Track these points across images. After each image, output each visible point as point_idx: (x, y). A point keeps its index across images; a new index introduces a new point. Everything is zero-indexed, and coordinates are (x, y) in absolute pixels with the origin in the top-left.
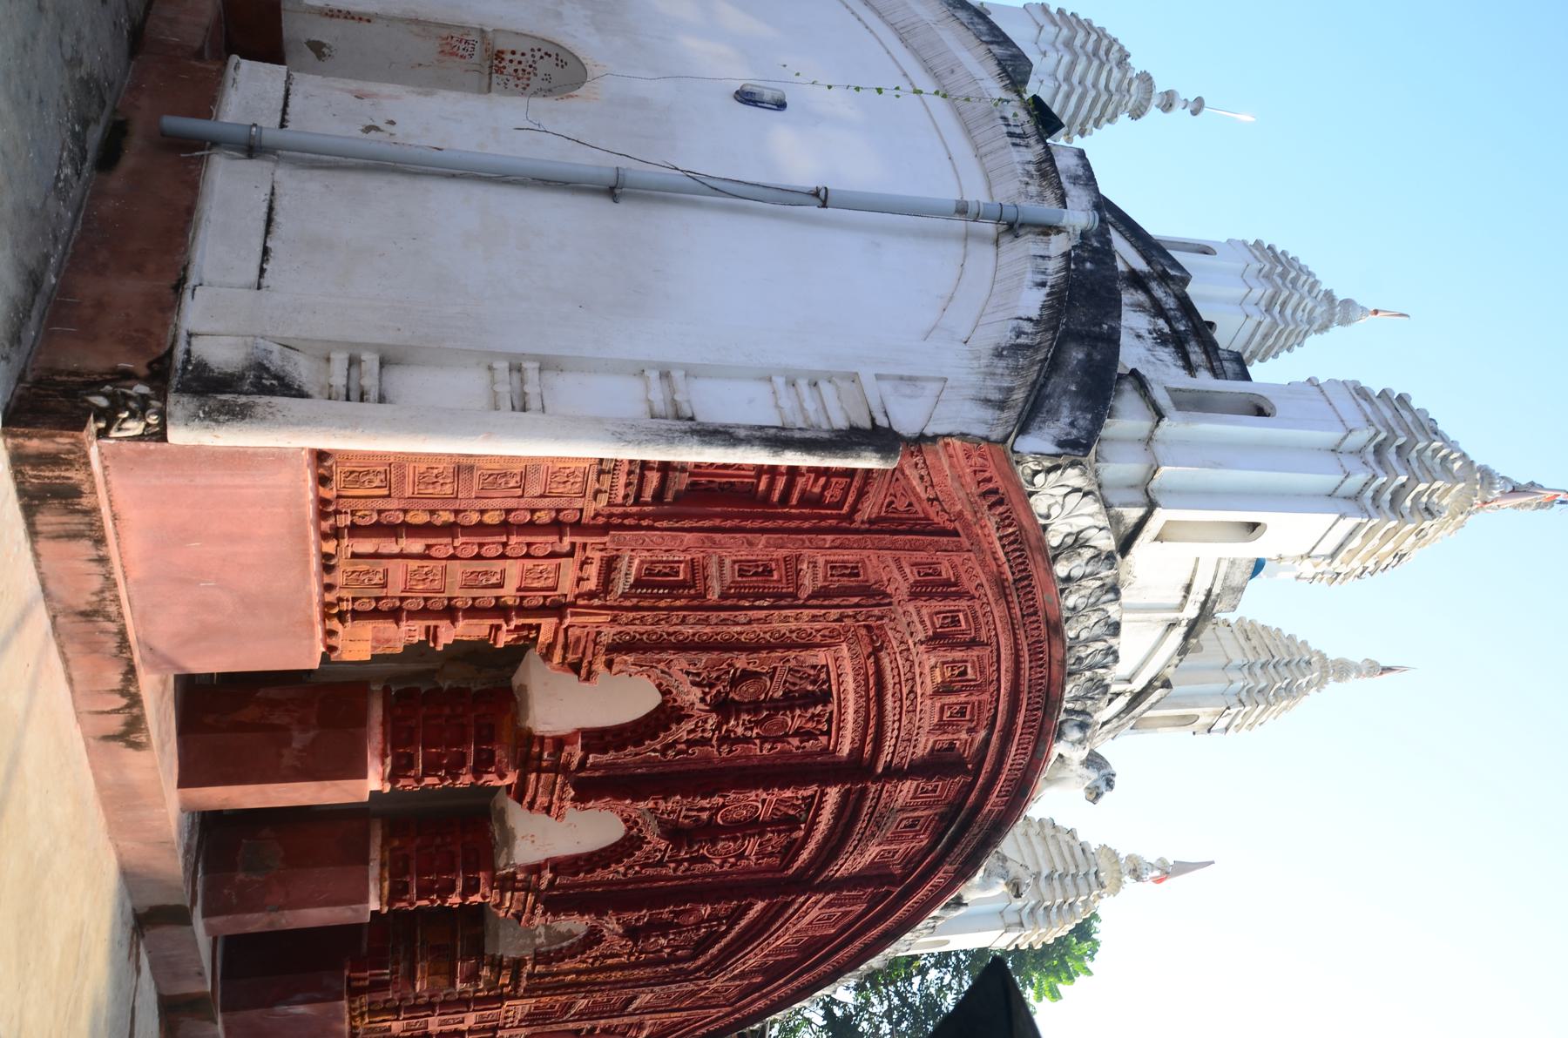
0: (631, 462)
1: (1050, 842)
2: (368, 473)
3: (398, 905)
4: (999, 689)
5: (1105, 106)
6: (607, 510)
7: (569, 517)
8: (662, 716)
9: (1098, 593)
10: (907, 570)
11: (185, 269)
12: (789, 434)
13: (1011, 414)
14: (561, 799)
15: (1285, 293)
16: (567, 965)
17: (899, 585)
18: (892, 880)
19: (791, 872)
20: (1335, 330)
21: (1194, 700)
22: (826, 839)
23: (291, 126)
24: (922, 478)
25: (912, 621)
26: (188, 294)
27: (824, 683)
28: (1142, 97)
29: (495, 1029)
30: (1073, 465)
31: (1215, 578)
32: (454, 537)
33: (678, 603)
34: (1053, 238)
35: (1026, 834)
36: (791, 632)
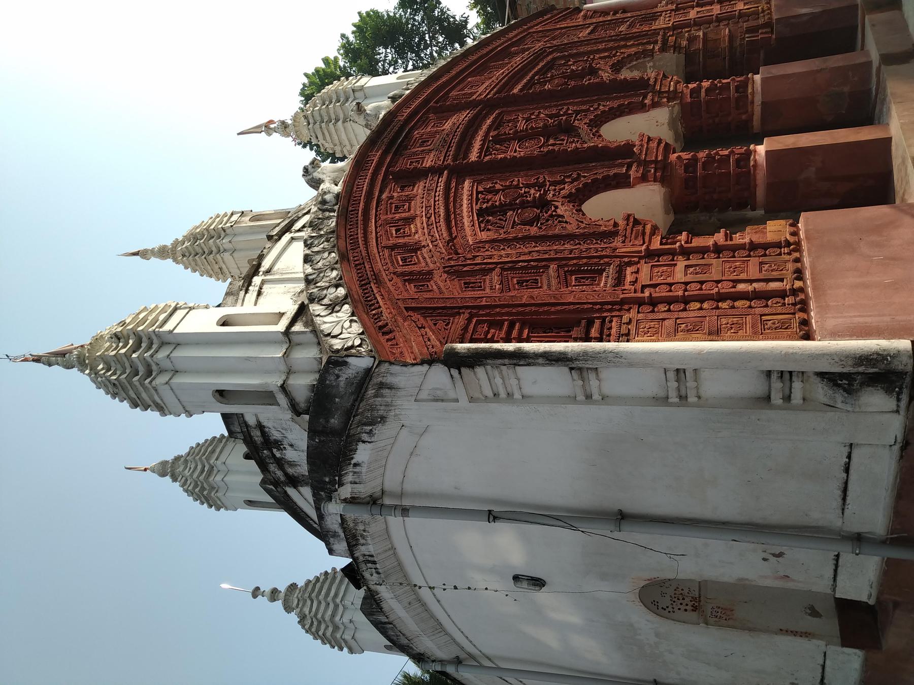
0: (609, 341)
1: (337, 142)
2: (776, 328)
5: (313, 590)
6: (622, 313)
8: (581, 197)
10: (435, 287)
11: (901, 457)
12: (512, 362)
13: (376, 380)
15: (201, 478)
16: (633, 50)
20: (170, 458)
21: (252, 230)
22: (476, 132)
23: (832, 555)
24: (429, 340)
26: (899, 439)
27: (482, 222)
28: (292, 598)
29: (677, 9)
30: (338, 351)
31: (243, 300)
33: (575, 261)
34: (349, 496)
35: (352, 146)
36: (504, 249)
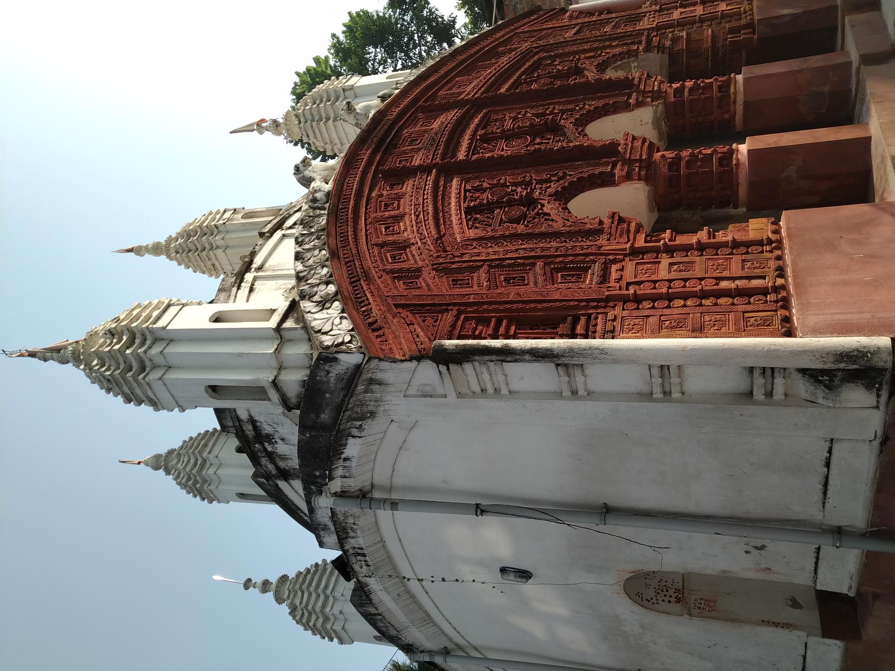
1: (328, 140)
2: (758, 325)
3: (725, 78)
4: (366, 220)
6: (607, 310)
7: (631, 305)
9: (309, 276)
10: (423, 284)
11: (881, 452)
13: (366, 376)
14: (626, 144)
15: (194, 471)
16: (617, 51)
17: (428, 278)
18: (423, 109)
19: (484, 111)
20: (163, 451)
21: (244, 227)
22: (464, 131)
23: (813, 548)
24: (418, 337)
25: (418, 256)
26: (879, 434)
27: (470, 219)
28: (283, 589)
30: (328, 347)
31: (236, 296)
32: (702, 290)
33: (561, 259)
34: (339, 490)
35: (342, 144)
36: (491, 247)
